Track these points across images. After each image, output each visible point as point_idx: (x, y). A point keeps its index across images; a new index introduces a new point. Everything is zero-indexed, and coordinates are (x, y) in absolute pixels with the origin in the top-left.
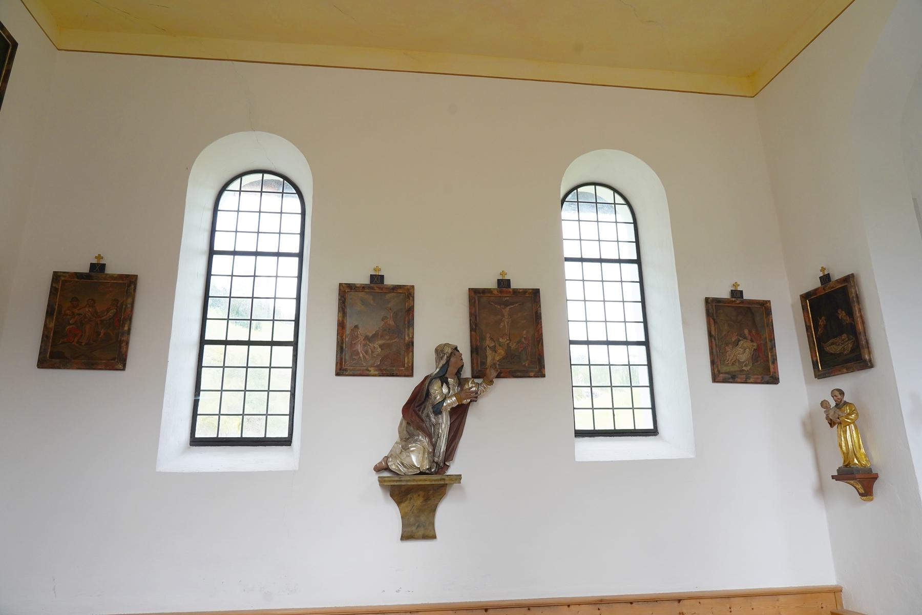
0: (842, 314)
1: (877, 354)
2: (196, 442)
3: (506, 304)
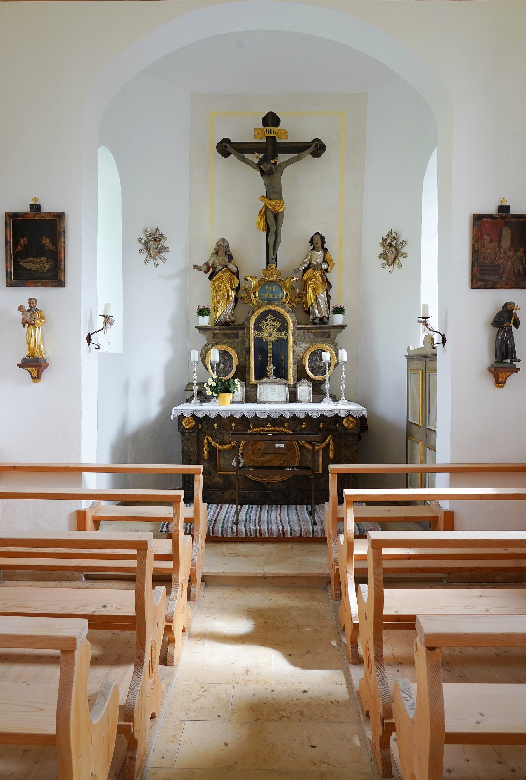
0: (46, 241)
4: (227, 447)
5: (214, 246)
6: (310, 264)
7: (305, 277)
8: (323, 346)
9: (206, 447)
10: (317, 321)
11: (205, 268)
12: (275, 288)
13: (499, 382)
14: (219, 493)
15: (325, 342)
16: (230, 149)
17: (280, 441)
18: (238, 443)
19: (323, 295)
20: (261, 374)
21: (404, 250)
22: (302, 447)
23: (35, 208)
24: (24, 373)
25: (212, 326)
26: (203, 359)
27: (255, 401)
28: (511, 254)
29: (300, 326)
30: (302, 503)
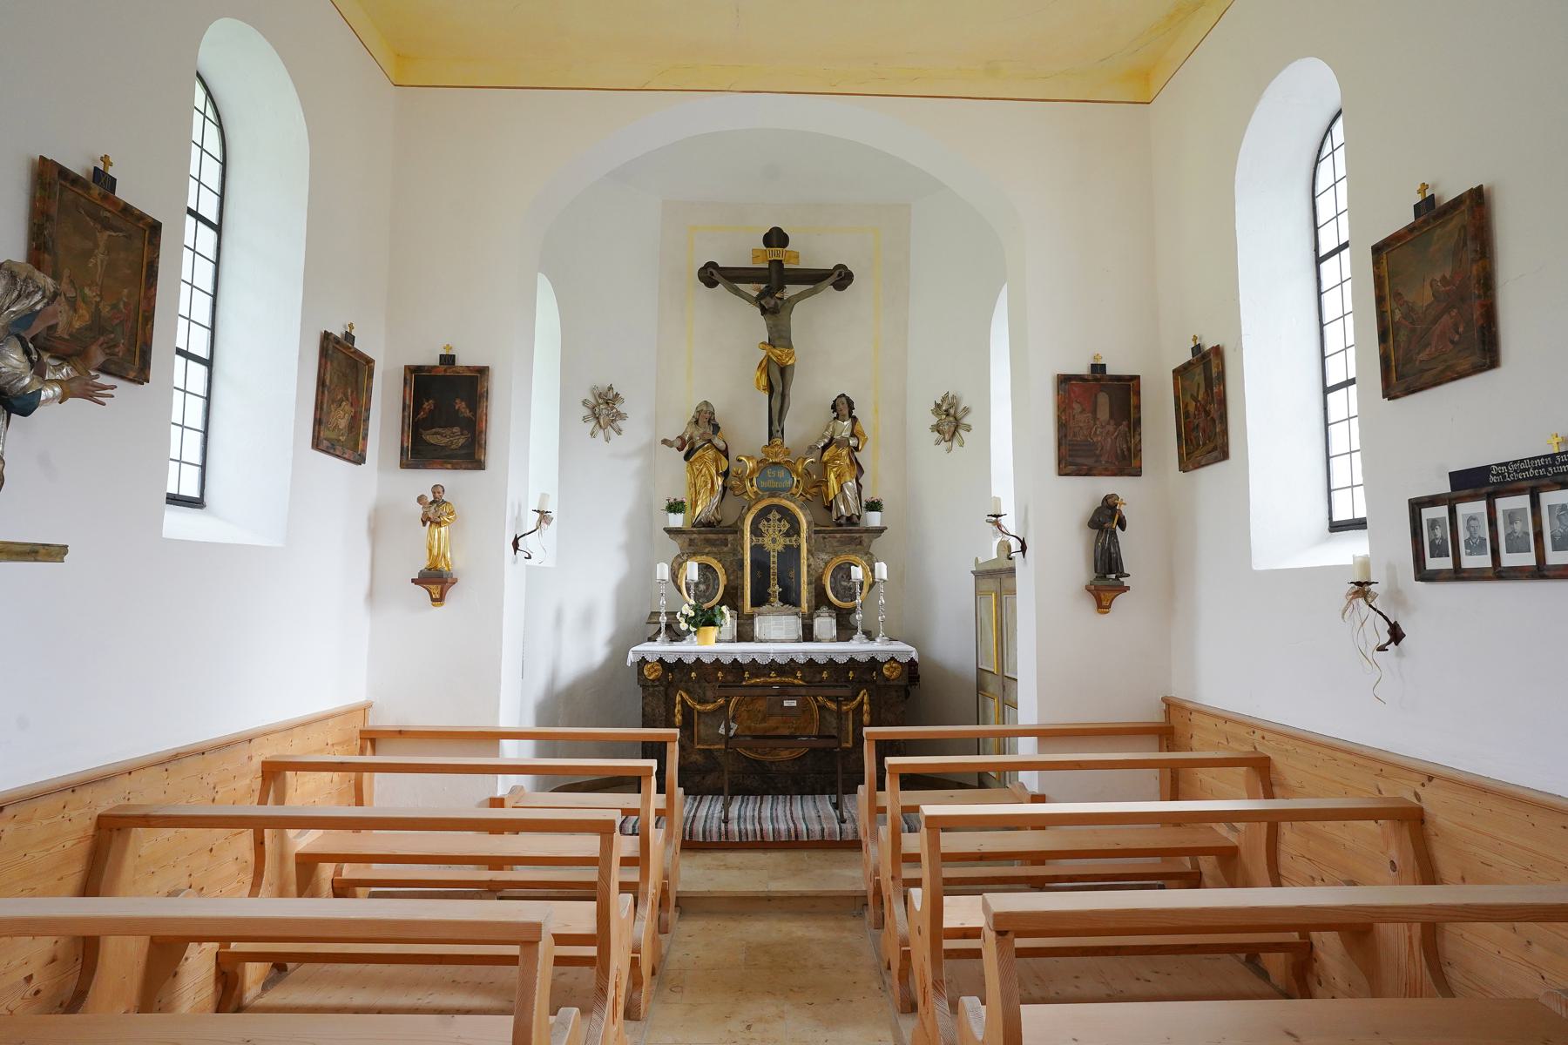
0: (461, 405)
1: (493, 454)
2: (1336, 527)
3: (107, 226)
4: (710, 707)
5: (693, 412)
6: (832, 439)
7: (825, 458)
8: (852, 558)
9: (678, 707)
10: (843, 521)
11: (679, 443)
12: (782, 473)
13: (1103, 606)
14: (697, 778)
15: (854, 552)
16: (717, 276)
17: (791, 697)
18: (728, 702)
19: (852, 484)
20: (760, 599)
21: (966, 421)
22: (822, 708)
23: (448, 360)
24: (421, 592)
25: (688, 527)
26: (675, 576)
27: (751, 639)
28: (1111, 428)
29: (817, 531)
30: (823, 793)
